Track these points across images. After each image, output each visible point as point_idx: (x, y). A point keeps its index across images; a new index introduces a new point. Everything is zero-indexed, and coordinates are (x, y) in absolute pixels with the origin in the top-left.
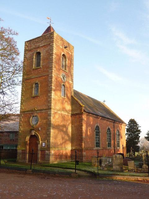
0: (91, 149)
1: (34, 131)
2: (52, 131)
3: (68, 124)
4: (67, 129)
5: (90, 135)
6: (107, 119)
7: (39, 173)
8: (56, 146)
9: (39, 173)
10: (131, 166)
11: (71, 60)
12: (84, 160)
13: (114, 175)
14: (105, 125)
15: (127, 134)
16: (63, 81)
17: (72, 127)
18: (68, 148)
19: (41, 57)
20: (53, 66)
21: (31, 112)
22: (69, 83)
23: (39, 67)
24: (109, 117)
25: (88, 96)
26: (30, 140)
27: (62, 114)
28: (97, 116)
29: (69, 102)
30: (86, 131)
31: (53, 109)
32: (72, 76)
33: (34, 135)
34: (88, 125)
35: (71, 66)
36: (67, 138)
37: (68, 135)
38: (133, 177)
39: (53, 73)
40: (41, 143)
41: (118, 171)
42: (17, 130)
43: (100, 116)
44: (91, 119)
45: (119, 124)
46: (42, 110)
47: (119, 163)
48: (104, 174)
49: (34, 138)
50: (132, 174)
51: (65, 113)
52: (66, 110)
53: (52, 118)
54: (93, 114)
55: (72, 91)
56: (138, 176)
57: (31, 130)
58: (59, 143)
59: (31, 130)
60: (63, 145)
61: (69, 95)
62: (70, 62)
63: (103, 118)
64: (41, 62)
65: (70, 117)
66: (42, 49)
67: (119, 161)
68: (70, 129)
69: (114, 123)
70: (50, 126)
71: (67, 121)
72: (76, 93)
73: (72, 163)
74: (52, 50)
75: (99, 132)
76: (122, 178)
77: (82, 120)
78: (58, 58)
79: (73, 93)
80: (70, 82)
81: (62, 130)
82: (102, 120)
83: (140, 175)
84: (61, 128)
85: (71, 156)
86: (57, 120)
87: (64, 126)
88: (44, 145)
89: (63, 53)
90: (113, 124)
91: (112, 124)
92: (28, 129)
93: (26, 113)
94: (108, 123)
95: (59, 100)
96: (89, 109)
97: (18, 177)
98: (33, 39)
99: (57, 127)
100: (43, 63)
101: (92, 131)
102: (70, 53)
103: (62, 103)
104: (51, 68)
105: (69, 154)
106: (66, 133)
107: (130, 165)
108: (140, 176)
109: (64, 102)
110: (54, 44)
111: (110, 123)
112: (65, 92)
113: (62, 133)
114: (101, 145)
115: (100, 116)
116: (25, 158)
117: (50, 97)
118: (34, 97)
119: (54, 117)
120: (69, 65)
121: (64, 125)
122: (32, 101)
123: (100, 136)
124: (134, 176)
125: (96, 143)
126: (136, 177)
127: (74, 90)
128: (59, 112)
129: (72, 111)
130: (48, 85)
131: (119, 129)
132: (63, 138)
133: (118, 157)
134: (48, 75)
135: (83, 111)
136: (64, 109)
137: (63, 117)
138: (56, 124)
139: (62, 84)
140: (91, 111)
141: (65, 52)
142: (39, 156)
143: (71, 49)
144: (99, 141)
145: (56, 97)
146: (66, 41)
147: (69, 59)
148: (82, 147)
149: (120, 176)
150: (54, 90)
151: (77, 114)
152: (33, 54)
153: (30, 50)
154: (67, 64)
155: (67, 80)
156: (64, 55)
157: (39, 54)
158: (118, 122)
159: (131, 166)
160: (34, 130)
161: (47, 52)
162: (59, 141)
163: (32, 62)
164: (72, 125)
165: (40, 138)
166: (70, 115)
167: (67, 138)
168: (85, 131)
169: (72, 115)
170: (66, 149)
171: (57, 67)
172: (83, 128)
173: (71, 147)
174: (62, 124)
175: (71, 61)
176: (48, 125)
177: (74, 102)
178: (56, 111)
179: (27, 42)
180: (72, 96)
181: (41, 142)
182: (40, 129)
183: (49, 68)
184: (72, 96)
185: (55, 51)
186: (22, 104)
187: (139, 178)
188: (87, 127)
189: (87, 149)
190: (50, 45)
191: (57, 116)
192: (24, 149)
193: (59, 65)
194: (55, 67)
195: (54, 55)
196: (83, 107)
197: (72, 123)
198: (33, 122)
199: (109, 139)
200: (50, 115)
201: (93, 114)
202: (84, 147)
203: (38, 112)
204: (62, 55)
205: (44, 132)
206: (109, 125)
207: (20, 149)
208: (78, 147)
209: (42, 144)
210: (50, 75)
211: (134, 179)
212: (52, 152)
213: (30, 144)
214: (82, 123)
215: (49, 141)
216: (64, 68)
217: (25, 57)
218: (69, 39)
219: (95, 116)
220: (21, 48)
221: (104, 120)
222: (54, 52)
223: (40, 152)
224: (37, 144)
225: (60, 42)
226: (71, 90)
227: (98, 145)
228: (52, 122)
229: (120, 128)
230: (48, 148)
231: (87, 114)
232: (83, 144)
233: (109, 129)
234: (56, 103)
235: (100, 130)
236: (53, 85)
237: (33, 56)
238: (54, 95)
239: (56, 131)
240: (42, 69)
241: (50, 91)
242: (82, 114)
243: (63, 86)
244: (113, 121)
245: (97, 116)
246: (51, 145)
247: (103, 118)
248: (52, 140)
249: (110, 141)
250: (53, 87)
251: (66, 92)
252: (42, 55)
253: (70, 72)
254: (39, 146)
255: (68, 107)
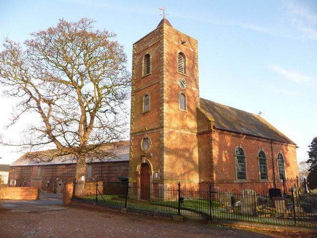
0: (229, 182)
1: (145, 158)
2: (167, 158)
3: (192, 146)
4: (191, 154)
5: (227, 161)
6: (256, 138)
7: (134, 213)
8: (172, 177)
9: (134, 213)
10: (281, 208)
11: (194, 58)
12: (216, 197)
13: (236, 220)
14: (254, 147)
15: (310, 160)
16: (182, 88)
17: (199, 151)
18: (195, 180)
19: (151, 61)
20: (164, 70)
21: (141, 134)
22: (191, 91)
23: (149, 74)
24: (261, 135)
25: (231, 108)
26: (141, 170)
27: (181, 134)
28: (238, 134)
29: (193, 117)
30: (220, 156)
31: (167, 127)
32: (196, 80)
33: (146, 163)
34: (222, 147)
35: (193, 67)
36: (191, 166)
37: (193, 162)
38: (267, 226)
39: (164, 79)
40: (153, 173)
41: (249, 215)
42: (128, 159)
43: (244, 134)
44: (228, 138)
45: (282, 145)
46: (153, 129)
47: (251, 203)
48: (218, 219)
49: (145, 166)
50: (275, 221)
51: (186, 132)
52: (188, 128)
53: (165, 139)
54: (231, 132)
55: (198, 100)
56: (276, 225)
57: (141, 156)
58: (179, 174)
59: (142, 156)
60: (186, 175)
61: (193, 107)
62: (191, 62)
63: (250, 136)
64: (151, 67)
65: (195, 137)
66: (151, 50)
67: (251, 200)
68: (196, 154)
69: (271, 143)
70: (163, 151)
71: (191, 142)
72: (209, 105)
73: (199, 202)
74: (162, 49)
75: (243, 158)
76: (247, 227)
77: (210, 140)
78: (172, 58)
79: (199, 104)
80: (194, 89)
81: (184, 156)
82: (247, 140)
83: (283, 223)
84: (181, 153)
85: (199, 192)
86: (174, 142)
87: (186, 150)
88: (156, 177)
89: (179, 51)
90: (270, 145)
91: (268, 145)
92: (138, 155)
93: (136, 135)
94: (261, 143)
95: (176, 115)
96: (223, 125)
97: (105, 217)
98: (141, 39)
99: (174, 152)
100: (152, 68)
101: (230, 156)
102: (192, 50)
103: (182, 119)
104: (161, 73)
105: (196, 189)
106: (190, 159)
107: (279, 207)
108: (279, 225)
109: (185, 116)
110: (165, 40)
111: (264, 143)
112: (185, 104)
113: (183, 159)
114: (247, 176)
115: (244, 134)
116: (136, 194)
117: (161, 112)
118: (144, 113)
119: (168, 139)
120: (191, 66)
121: (186, 149)
122: (143, 119)
123: (266, 165)
124: (269, 224)
125: (240, 173)
126: (272, 227)
127: (202, 99)
128: (177, 131)
129: (198, 128)
130: (158, 95)
131: (283, 153)
132: (184, 167)
133: (248, 193)
134: (159, 83)
135: (212, 128)
136: (185, 127)
137: (184, 139)
138: (172, 148)
139: (181, 92)
140: (227, 127)
141: (183, 49)
142: (152, 191)
143: (192, 45)
144: (243, 170)
145: (171, 110)
146: (184, 34)
147: (190, 59)
148: (212, 179)
149: (246, 224)
150: (168, 102)
151: (204, 133)
152: (142, 58)
153: (138, 54)
154: (187, 65)
155: (189, 87)
156: (180, 53)
157: (148, 56)
158: (279, 143)
159: (281, 208)
160: (144, 156)
161: (156, 52)
162: (179, 169)
163: (141, 68)
164: (199, 148)
165: (152, 167)
166: (196, 134)
167: (192, 167)
168: (217, 156)
169: (199, 134)
170: (190, 182)
171: (171, 70)
172: (213, 152)
173: (198, 179)
174: (182, 147)
175: (193, 61)
176: (161, 149)
177: (200, 117)
178: (171, 130)
179: (135, 44)
180: (197, 109)
181: (153, 172)
182: (152, 155)
183: (159, 73)
184: (197, 109)
185: (166, 50)
186: (131, 123)
187: (278, 229)
188: (221, 150)
189: (221, 182)
190: (160, 43)
191: (173, 137)
192: (135, 181)
193: (174, 68)
194: (168, 71)
195: (164, 54)
196: (213, 122)
197: (199, 145)
198: (145, 148)
199: (263, 168)
200: (162, 136)
201: (231, 132)
202: (216, 178)
203: (149, 132)
204: (178, 54)
205: (157, 158)
206: (264, 147)
207: (131, 180)
208: (208, 180)
209: (154, 174)
210: (161, 83)
211: (268, 230)
212: (168, 185)
213: (142, 174)
214: (211, 146)
215: (162, 171)
216: (183, 72)
217: (134, 64)
218: (185, 30)
219: (233, 134)
220: (129, 52)
221: (252, 139)
222: (165, 51)
223: (152, 186)
224: (149, 175)
225: (174, 37)
226: (195, 100)
227: (242, 175)
228: (165, 145)
229: (285, 151)
230: (162, 180)
231: (219, 131)
232: (214, 175)
233: (262, 153)
234: (171, 119)
235: (245, 154)
236: (165, 95)
237: (142, 61)
238: (168, 108)
239: (174, 157)
240: (152, 76)
241: (160, 104)
242: (210, 132)
243: (178, 95)
244: (270, 141)
245: (238, 134)
246: (166, 176)
247: (250, 136)
248: (166, 169)
249: (265, 170)
250: (166, 98)
251: (187, 103)
252: (151, 57)
253: (193, 75)
254: (152, 177)
255: (192, 124)
